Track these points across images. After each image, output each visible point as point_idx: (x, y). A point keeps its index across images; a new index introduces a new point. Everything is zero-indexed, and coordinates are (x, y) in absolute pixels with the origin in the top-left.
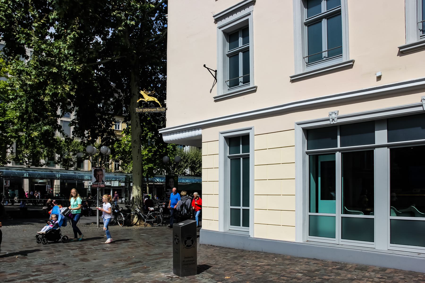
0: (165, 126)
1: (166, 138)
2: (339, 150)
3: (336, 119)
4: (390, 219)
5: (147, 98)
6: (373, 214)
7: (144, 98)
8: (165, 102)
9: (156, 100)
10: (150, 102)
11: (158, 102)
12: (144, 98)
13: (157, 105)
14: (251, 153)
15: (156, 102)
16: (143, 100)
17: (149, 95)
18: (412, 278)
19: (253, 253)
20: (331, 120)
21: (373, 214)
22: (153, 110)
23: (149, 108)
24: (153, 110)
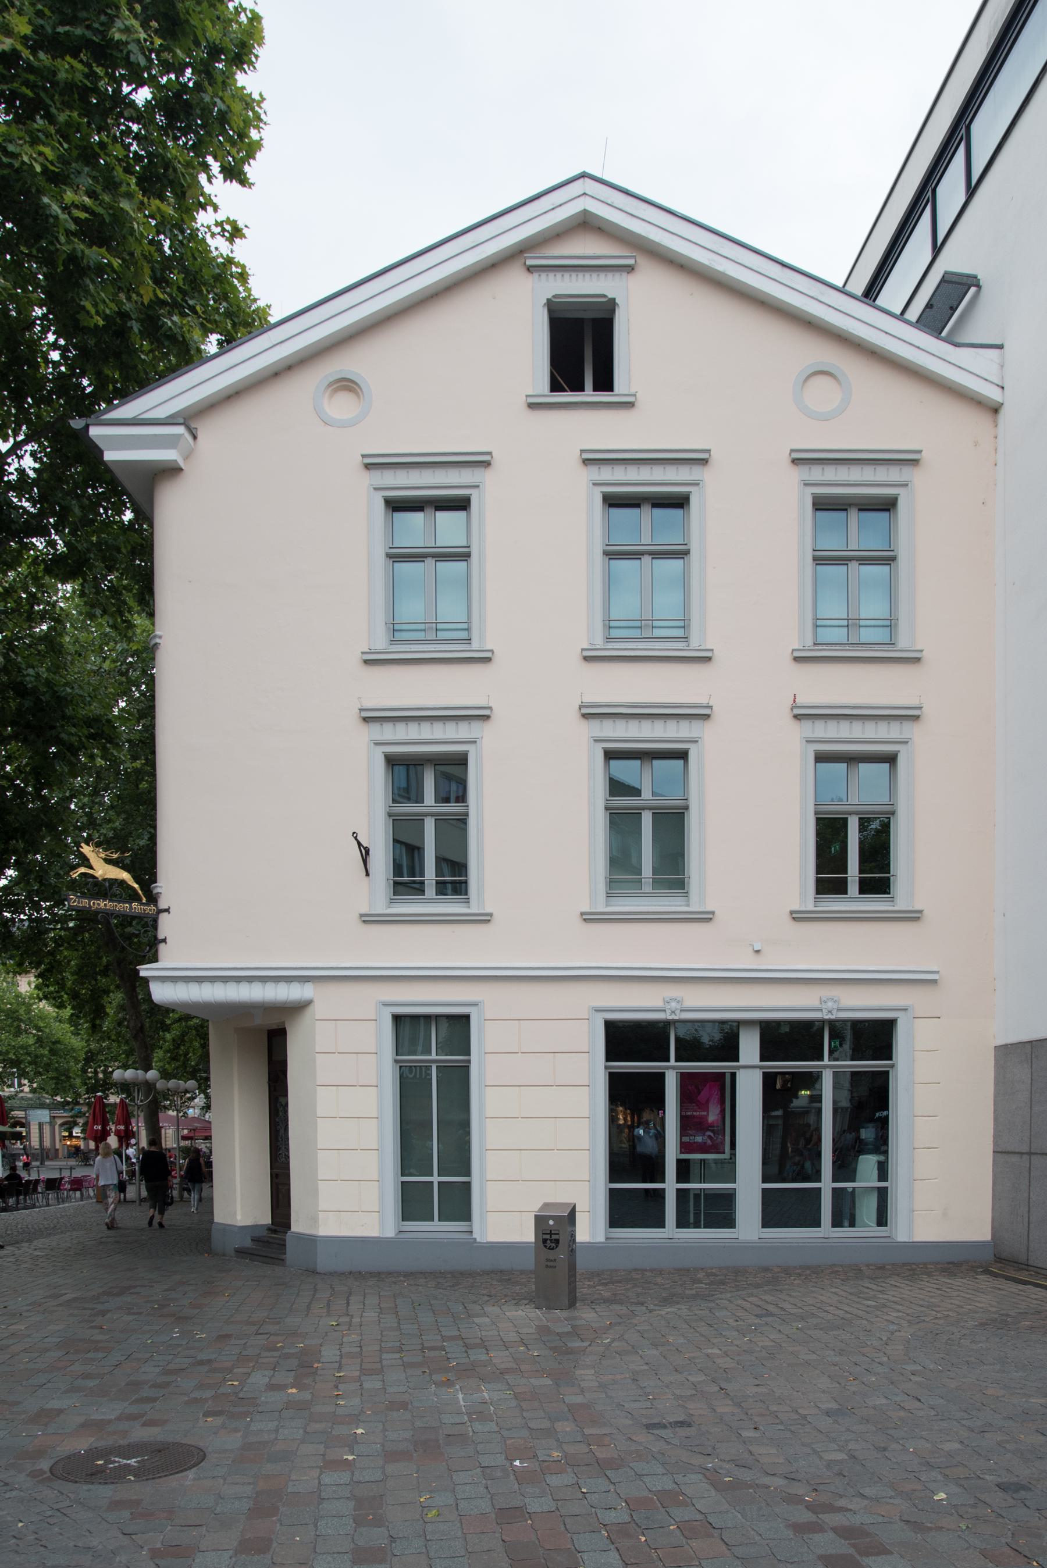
0: (155, 959)
1: (161, 993)
2: (673, 1068)
3: (678, 1012)
4: (402, 1182)
5: (103, 870)
6: (764, 1190)
7: (91, 868)
8: (155, 891)
9: (125, 876)
10: (114, 882)
11: (136, 886)
12: (91, 868)
13: (134, 897)
14: (474, 1057)
15: (130, 883)
16: (91, 872)
17: (108, 861)
18: (245, 1344)
19: (906, 1288)
20: (668, 1012)
21: (764, 1190)
22: (124, 907)
23: (110, 901)
24: (124, 907)
